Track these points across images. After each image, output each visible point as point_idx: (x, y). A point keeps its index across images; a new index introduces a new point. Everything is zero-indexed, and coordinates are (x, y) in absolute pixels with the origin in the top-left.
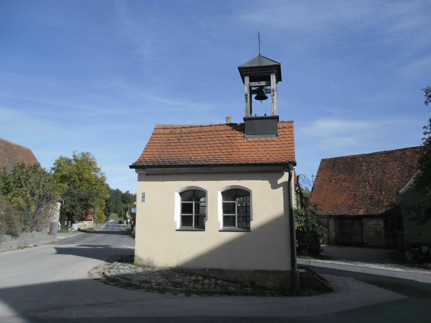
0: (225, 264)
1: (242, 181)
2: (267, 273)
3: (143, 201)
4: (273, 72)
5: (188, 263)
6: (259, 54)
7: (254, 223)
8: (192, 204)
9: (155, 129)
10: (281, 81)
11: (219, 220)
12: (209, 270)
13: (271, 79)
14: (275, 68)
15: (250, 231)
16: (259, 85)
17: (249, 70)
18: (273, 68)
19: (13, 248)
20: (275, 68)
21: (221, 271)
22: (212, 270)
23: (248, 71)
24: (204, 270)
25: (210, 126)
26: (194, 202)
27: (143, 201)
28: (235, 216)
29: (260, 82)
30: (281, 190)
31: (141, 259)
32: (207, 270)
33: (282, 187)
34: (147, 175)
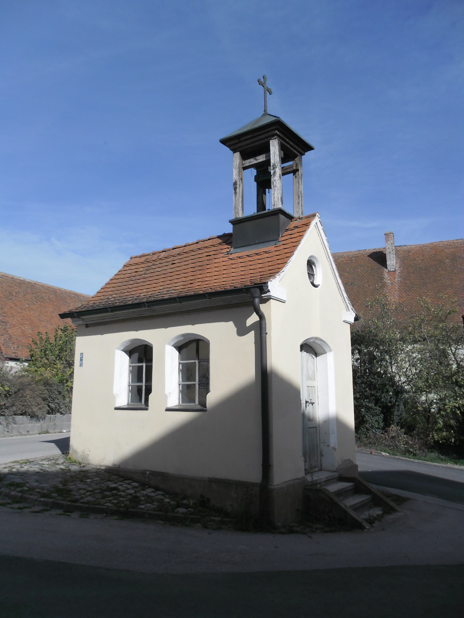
0: (170, 467)
1: (197, 326)
2: (226, 484)
3: (81, 365)
4: (273, 136)
5: (127, 461)
6: (265, 111)
7: (213, 398)
8: (142, 366)
9: (131, 258)
10: (308, 148)
11: (116, 390)
12: (149, 474)
13: (271, 148)
14: (274, 127)
15: (205, 411)
16: (255, 162)
17: (237, 141)
18: (271, 128)
19: (30, 433)
20: (274, 127)
21: (163, 476)
22: (154, 474)
23: (237, 143)
24: (143, 473)
25: (197, 243)
26: (144, 365)
27: (81, 365)
28: (142, 386)
29: (258, 158)
30: (251, 336)
31: (75, 452)
32: (148, 473)
33: (253, 332)
34: (87, 326)
